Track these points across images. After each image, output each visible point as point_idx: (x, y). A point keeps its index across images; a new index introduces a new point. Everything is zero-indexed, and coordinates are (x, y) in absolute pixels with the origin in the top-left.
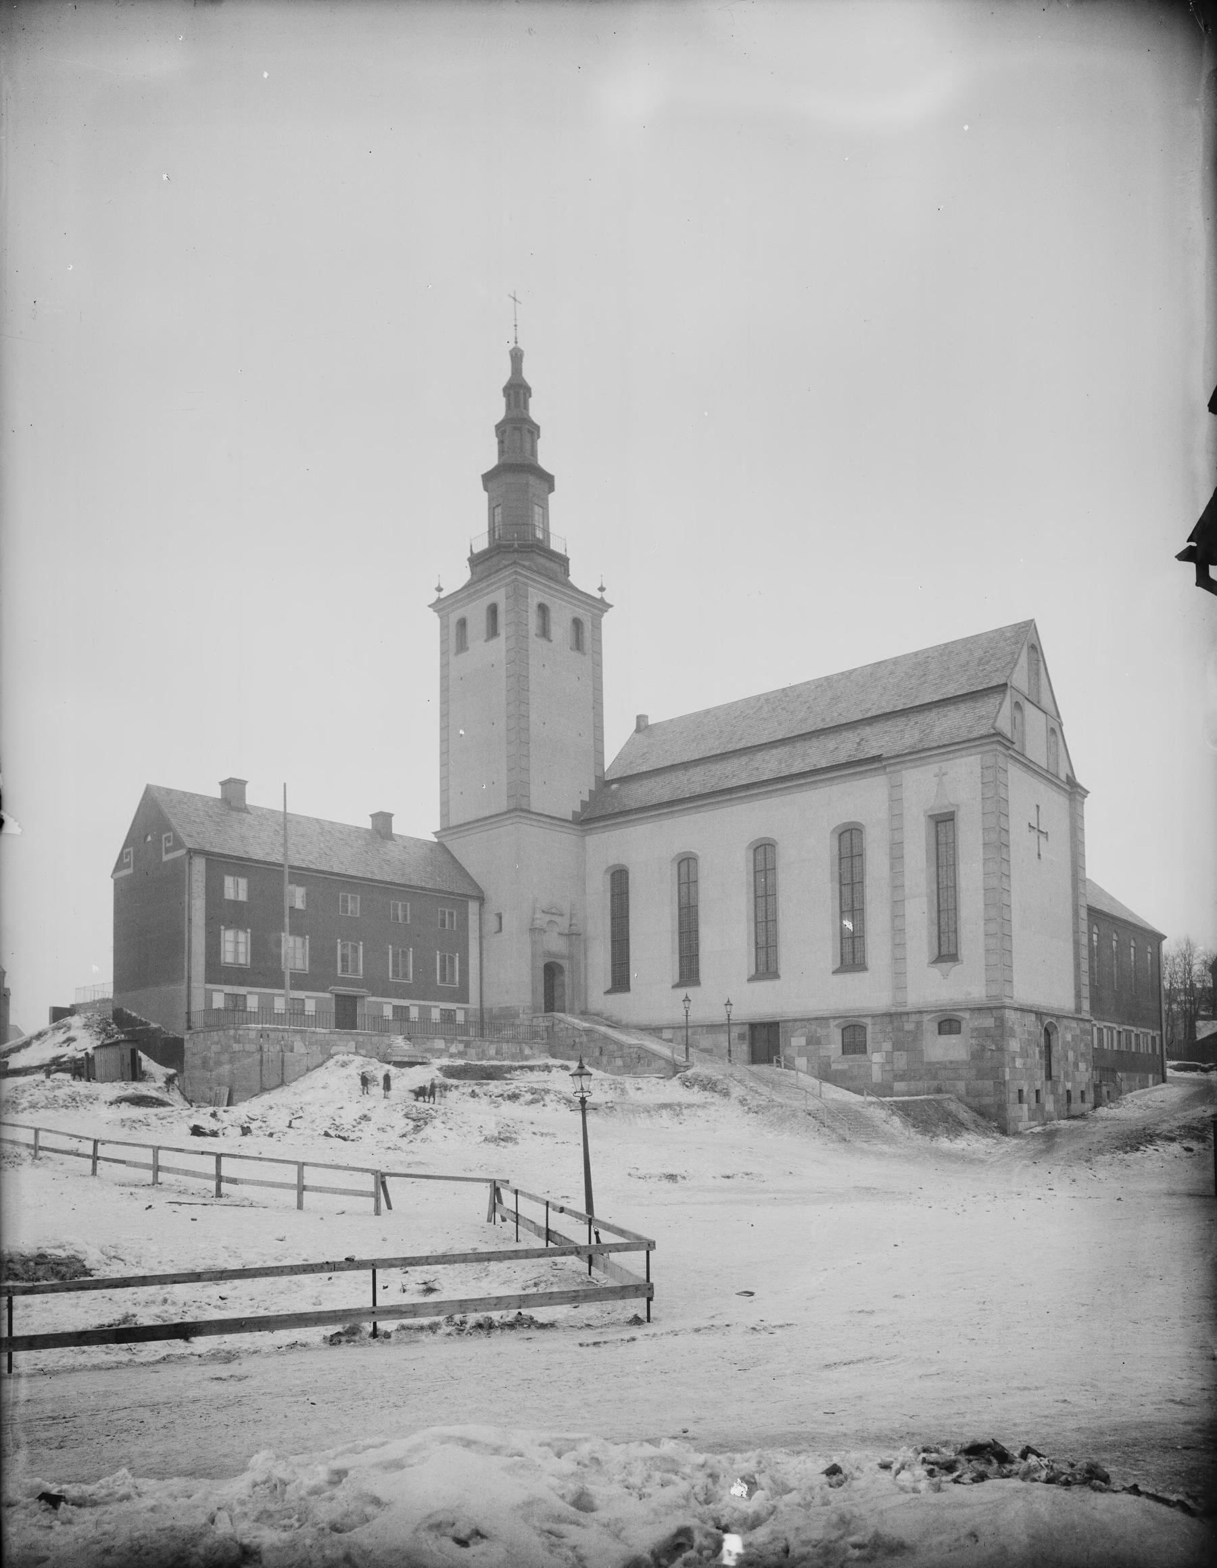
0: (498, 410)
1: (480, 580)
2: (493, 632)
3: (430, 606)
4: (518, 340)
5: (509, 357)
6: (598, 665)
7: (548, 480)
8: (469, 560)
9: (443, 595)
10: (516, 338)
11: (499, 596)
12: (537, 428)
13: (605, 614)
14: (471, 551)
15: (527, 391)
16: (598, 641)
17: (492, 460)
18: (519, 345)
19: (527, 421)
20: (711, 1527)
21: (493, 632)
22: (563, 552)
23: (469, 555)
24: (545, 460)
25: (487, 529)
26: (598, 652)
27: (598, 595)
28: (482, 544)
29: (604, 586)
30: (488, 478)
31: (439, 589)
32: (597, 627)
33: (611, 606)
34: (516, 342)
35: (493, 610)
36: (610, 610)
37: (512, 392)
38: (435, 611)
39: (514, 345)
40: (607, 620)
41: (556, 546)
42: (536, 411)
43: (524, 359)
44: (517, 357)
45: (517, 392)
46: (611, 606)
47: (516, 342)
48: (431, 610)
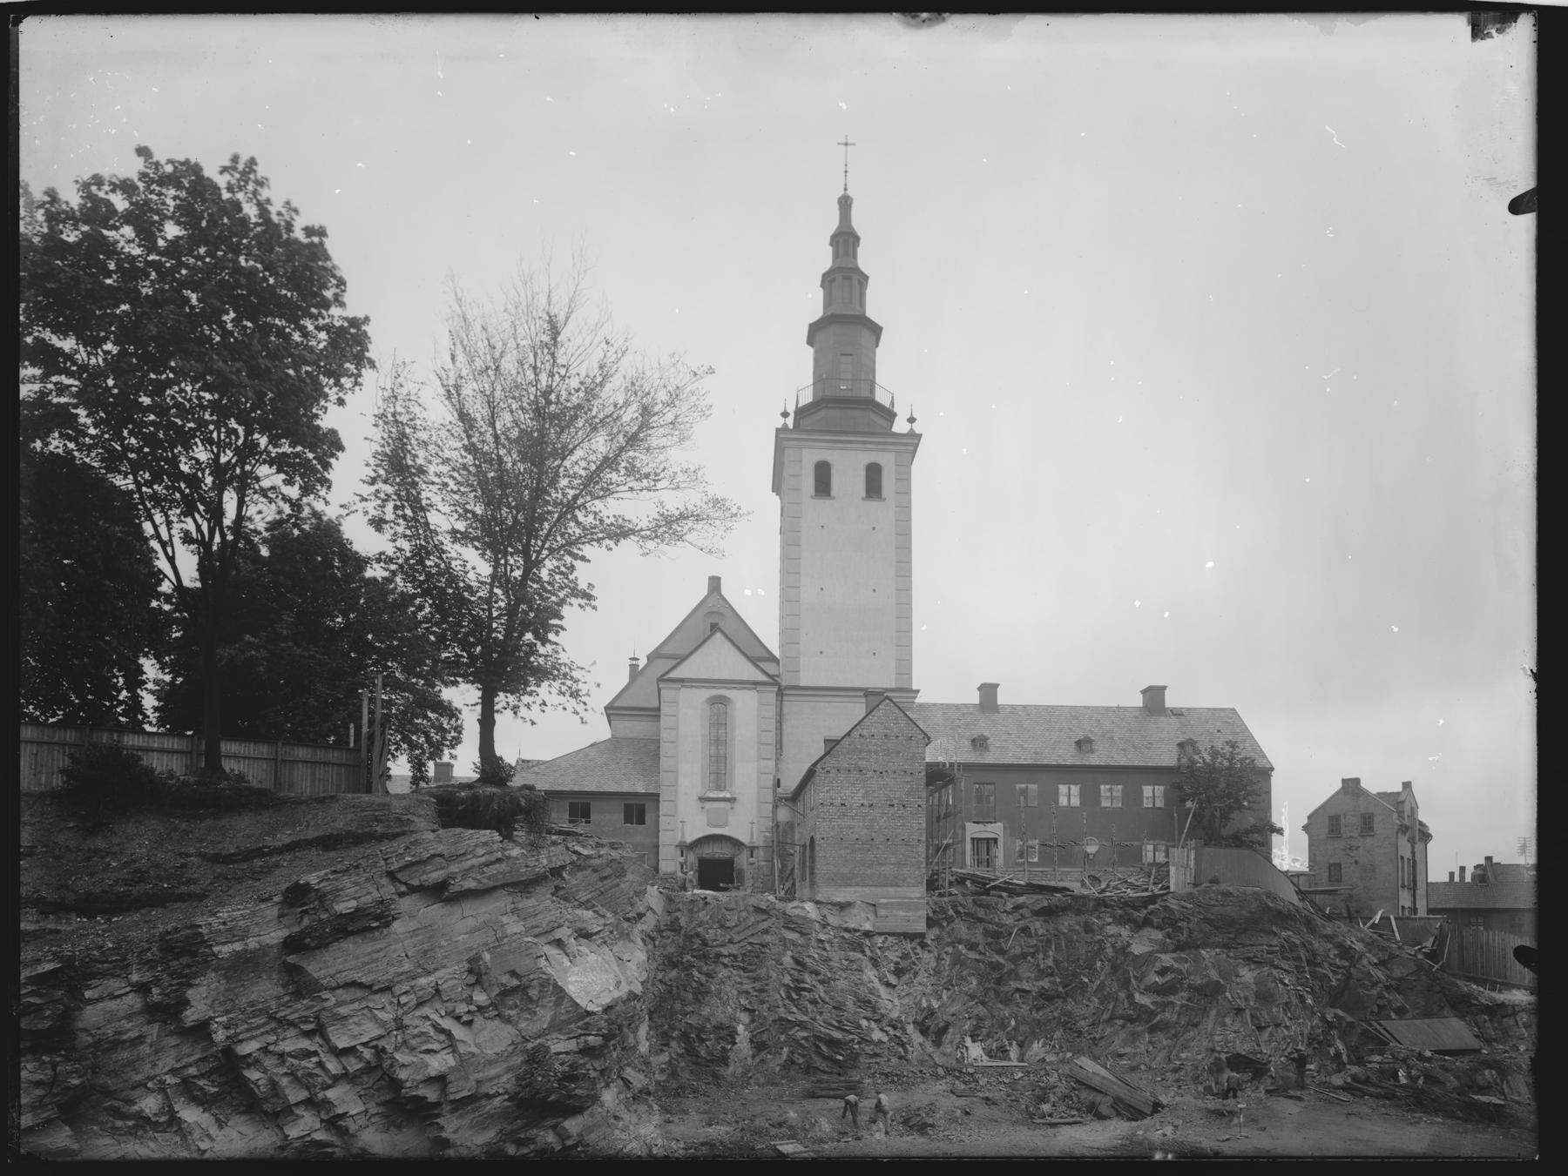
5: (836, 207)
7: (876, 330)
10: (846, 185)
12: (866, 278)
15: (856, 239)
16: (905, 492)
17: (816, 311)
18: (849, 192)
19: (857, 270)
20: (537, 1135)
22: (887, 404)
25: (810, 381)
28: (807, 398)
29: (915, 416)
30: (815, 330)
32: (905, 479)
34: (846, 189)
37: (841, 240)
41: (881, 398)
44: (845, 204)
45: (845, 240)
47: (846, 189)
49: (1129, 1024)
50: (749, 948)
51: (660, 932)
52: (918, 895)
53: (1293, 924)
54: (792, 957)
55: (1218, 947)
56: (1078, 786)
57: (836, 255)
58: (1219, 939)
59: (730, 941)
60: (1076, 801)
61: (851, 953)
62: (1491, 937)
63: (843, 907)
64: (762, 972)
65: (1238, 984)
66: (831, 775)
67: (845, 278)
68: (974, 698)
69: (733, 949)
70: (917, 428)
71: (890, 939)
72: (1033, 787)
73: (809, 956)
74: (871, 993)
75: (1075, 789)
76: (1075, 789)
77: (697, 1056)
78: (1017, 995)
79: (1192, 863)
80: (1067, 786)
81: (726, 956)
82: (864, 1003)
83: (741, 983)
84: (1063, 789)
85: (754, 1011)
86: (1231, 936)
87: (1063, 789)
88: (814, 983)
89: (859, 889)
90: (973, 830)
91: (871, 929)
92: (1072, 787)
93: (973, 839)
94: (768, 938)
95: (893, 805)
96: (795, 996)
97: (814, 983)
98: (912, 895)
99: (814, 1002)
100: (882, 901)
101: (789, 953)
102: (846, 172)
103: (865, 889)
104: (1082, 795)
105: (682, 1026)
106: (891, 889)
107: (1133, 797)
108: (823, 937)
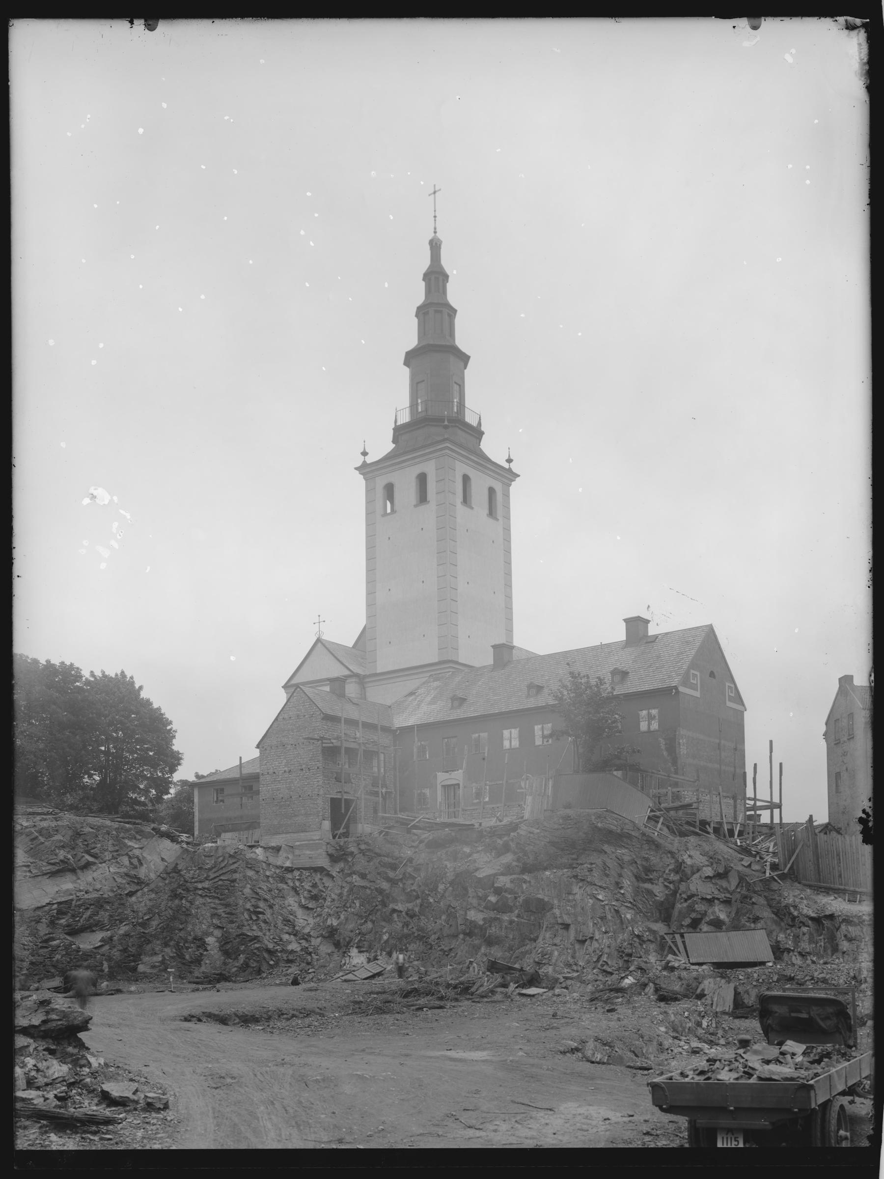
0: (419, 296)
1: (406, 453)
2: (423, 498)
3: (356, 469)
4: (437, 230)
6: (507, 530)
8: (393, 429)
9: (370, 459)
10: (435, 229)
11: (429, 468)
12: (455, 311)
13: (513, 483)
14: (396, 422)
16: (507, 507)
17: (412, 342)
21: (423, 498)
23: (393, 426)
24: (462, 342)
25: (408, 405)
26: (507, 517)
27: (506, 465)
28: (405, 418)
30: (410, 358)
31: (365, 454)
32: (507, 495)
33: (519, 476)
34: (435, 232)
35: (422, 479)
36: (518, 479)
38: (361, 474)
39: (433, 234)
40: (515, 488)
42: (454, 295)
43: (442, 246)
44: (435, 246)
46: (519, 476)
47: (435, 232)
48: (358, 472)
49: (468, 938)
50: (220, 883)
51: (168, 874)
52: (318, 838)
53: (629, 842)
54: (251, 888)
55: (565, 867)
56: (518, 729)
57: (428, 291)
58: (565, 860)
59: (206, 879)
60: (516, 743)
61: (279, 885)
62: (848, 842)
63: (277, 849)
64: (231, 900)
65: (569, 901)
66: (267, 752)
67: (436, 311)
68: (620, 634)
69: (206, 884)
70: (514, 467)
71: (304, 872)
72: (484, 735)
73: (260, 888)
74: (291, 914)
75: (515, 732)
76: (515, 732)
77: (184, 959)
78: (395, 915)
79: (550, 791)
80: (509, 731)
81: (200, 889)
82: (287, 921)
83: (216, 909)
84: (506, 733)
85: (223, 928)
86: (574, 856)
87: (506, 733)
88: (265, 908)
89: (284, 836)
90: (442, 778)
91: (290, 866)
92: (513, 730)
93: (444, 786)
94: (236, 876)
95: (302, 769)
96: (254, 918)
97: (265, 908)
98: (315, 838)
99: (265, 922)
100: (297, 843)
101: (249, 886)
102: (435, 217)
103: (288, 835)
104: (521, 737)
105: (176, 938)
106: (302, 834)
107: (526, 737)
108: (268, 873)
